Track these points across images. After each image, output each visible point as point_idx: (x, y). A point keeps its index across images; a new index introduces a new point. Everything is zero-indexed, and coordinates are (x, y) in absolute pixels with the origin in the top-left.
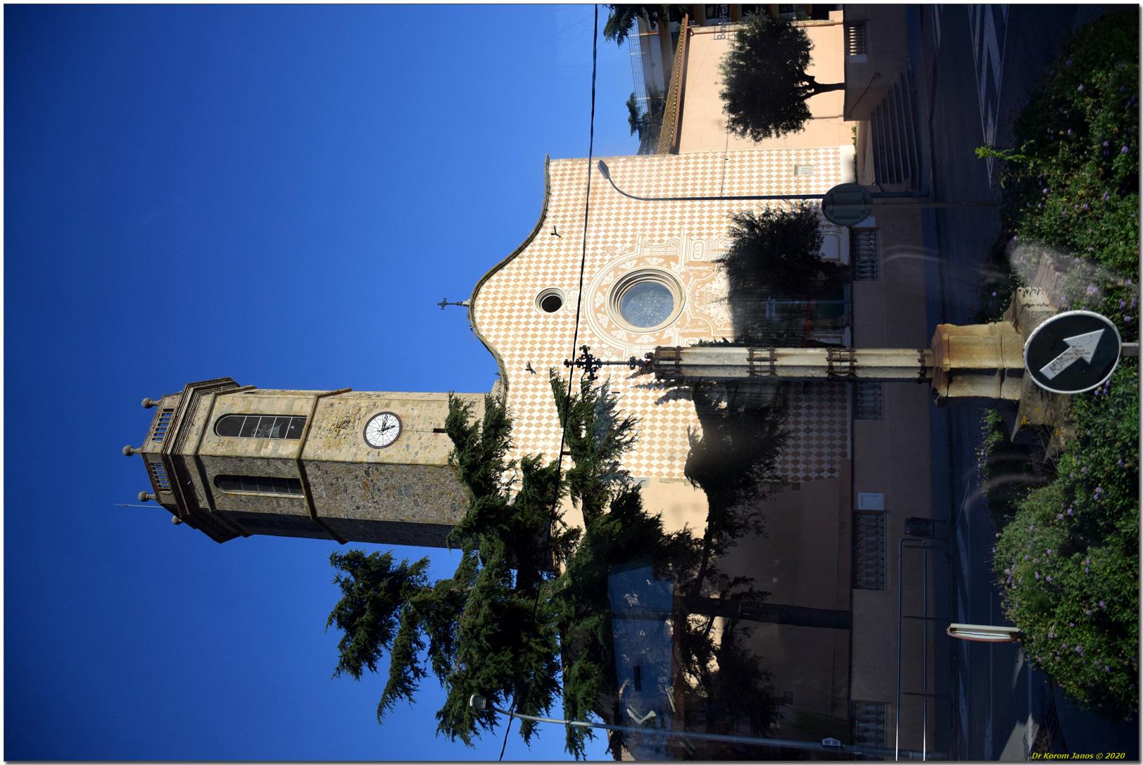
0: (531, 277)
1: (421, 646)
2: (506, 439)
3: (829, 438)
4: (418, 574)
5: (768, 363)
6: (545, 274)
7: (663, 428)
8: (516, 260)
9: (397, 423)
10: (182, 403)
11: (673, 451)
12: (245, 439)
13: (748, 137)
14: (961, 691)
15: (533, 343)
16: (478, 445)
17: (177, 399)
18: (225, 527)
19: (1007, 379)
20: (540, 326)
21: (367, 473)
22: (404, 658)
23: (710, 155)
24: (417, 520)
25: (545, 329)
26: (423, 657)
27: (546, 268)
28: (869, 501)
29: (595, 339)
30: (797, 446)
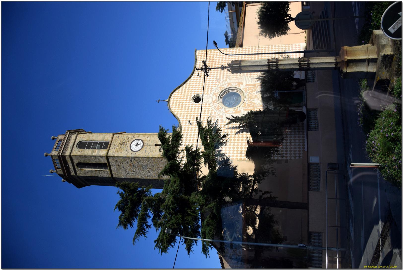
0: (190, 91)
1: (149, 217)
2: (180, 142)
3: (298, 145)
4: (148, 192)
5: (275, 64)
6: (195, 90)
7: (238, 143)
8: (185, 85)
9: (142, 143)
10: (65, 137)
11: (241, 151)
12: (88, 149)
13: (267, 37)
14: (351, 224)
15: (191, 114)
16: (170, 143)
17: (64, 136)
18: (81, 182)
19: (370, 63)
20: (193, 108)
21: (131, 161)
22: (142, 220)
23: (254, 47)
24: (149, 178)
25: (195, 109)
26: (150, 221)
27: (195, 87)
28: (314, 159)
29: (213, 112)
30: (287, 143)
